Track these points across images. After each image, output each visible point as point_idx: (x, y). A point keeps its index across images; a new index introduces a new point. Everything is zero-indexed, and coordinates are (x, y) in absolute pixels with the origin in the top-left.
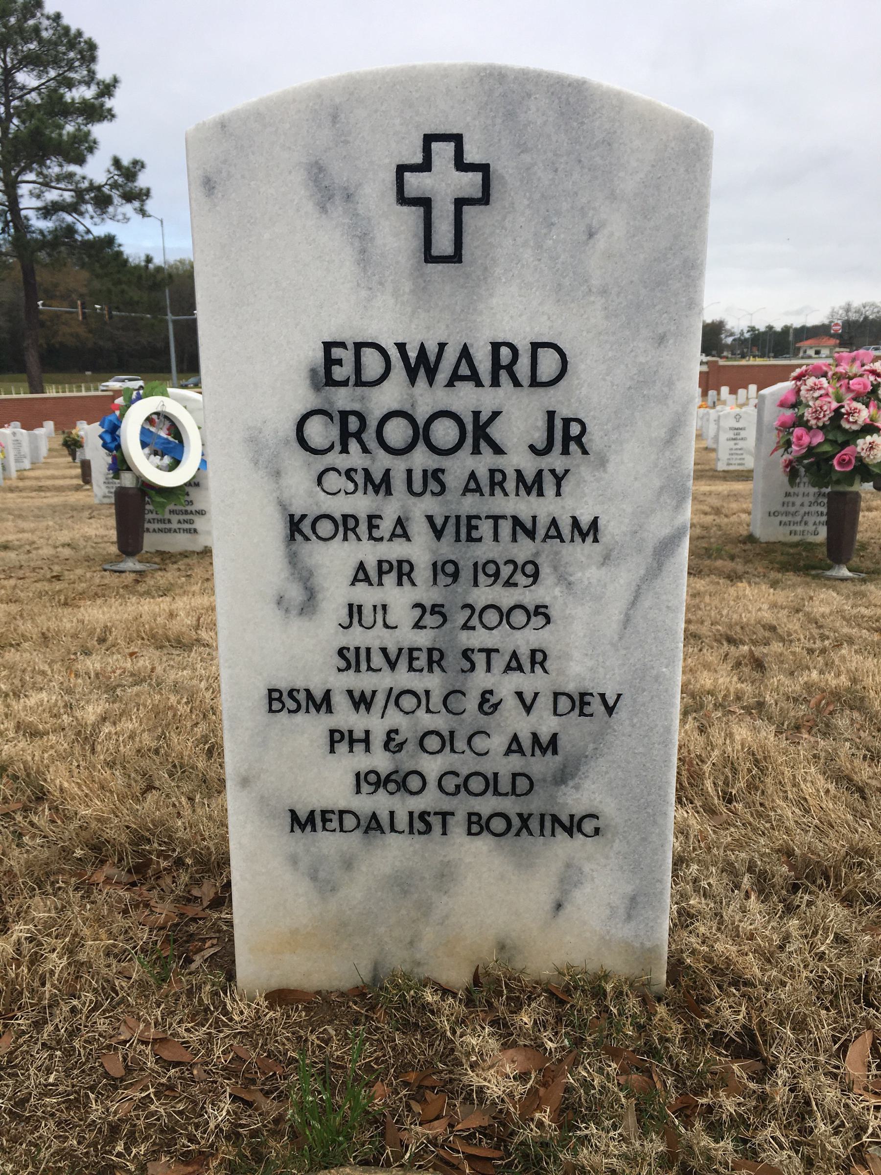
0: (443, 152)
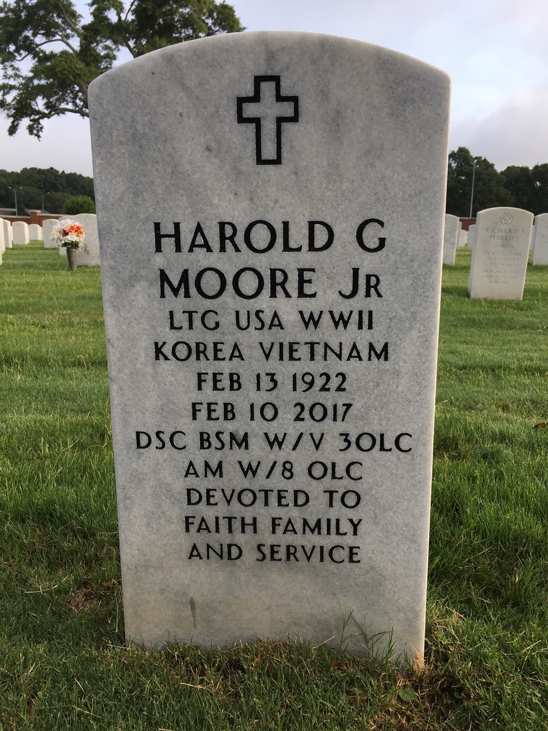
0: (268, 88)
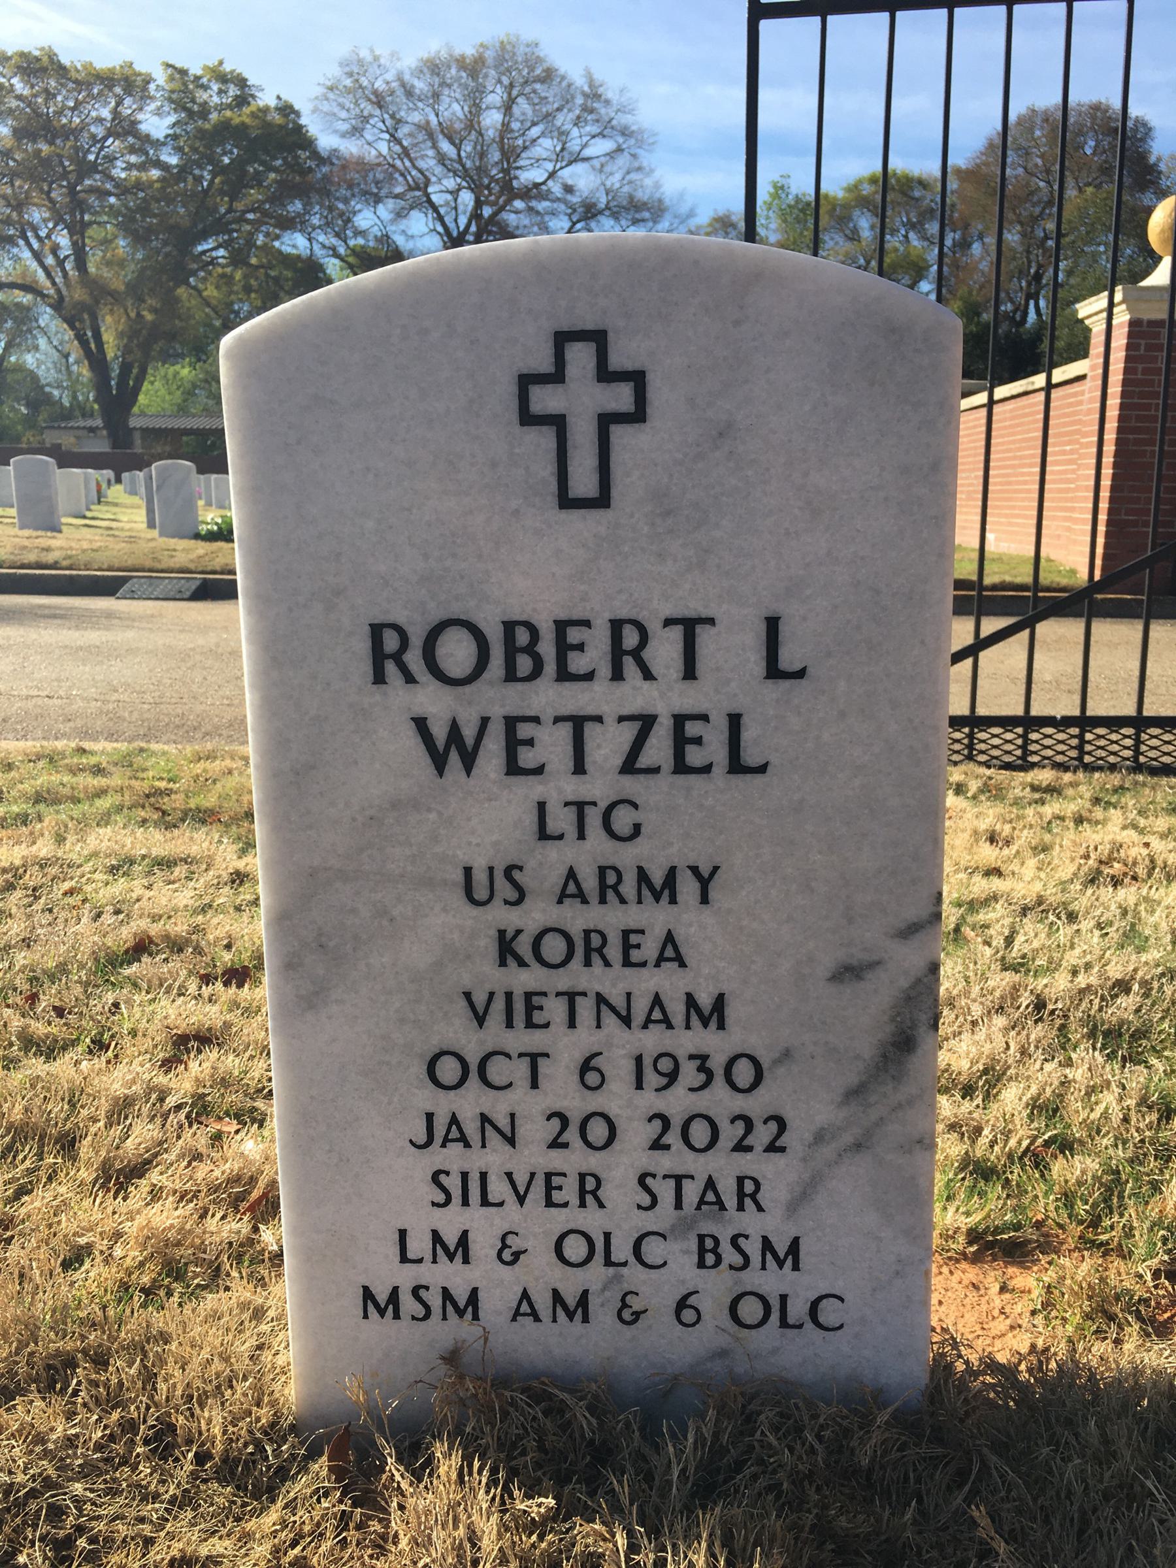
0: (580, 357)
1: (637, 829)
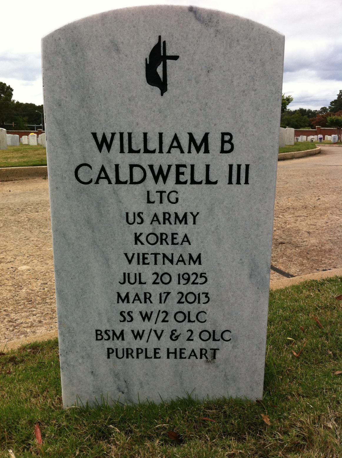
1: (177, 199)
